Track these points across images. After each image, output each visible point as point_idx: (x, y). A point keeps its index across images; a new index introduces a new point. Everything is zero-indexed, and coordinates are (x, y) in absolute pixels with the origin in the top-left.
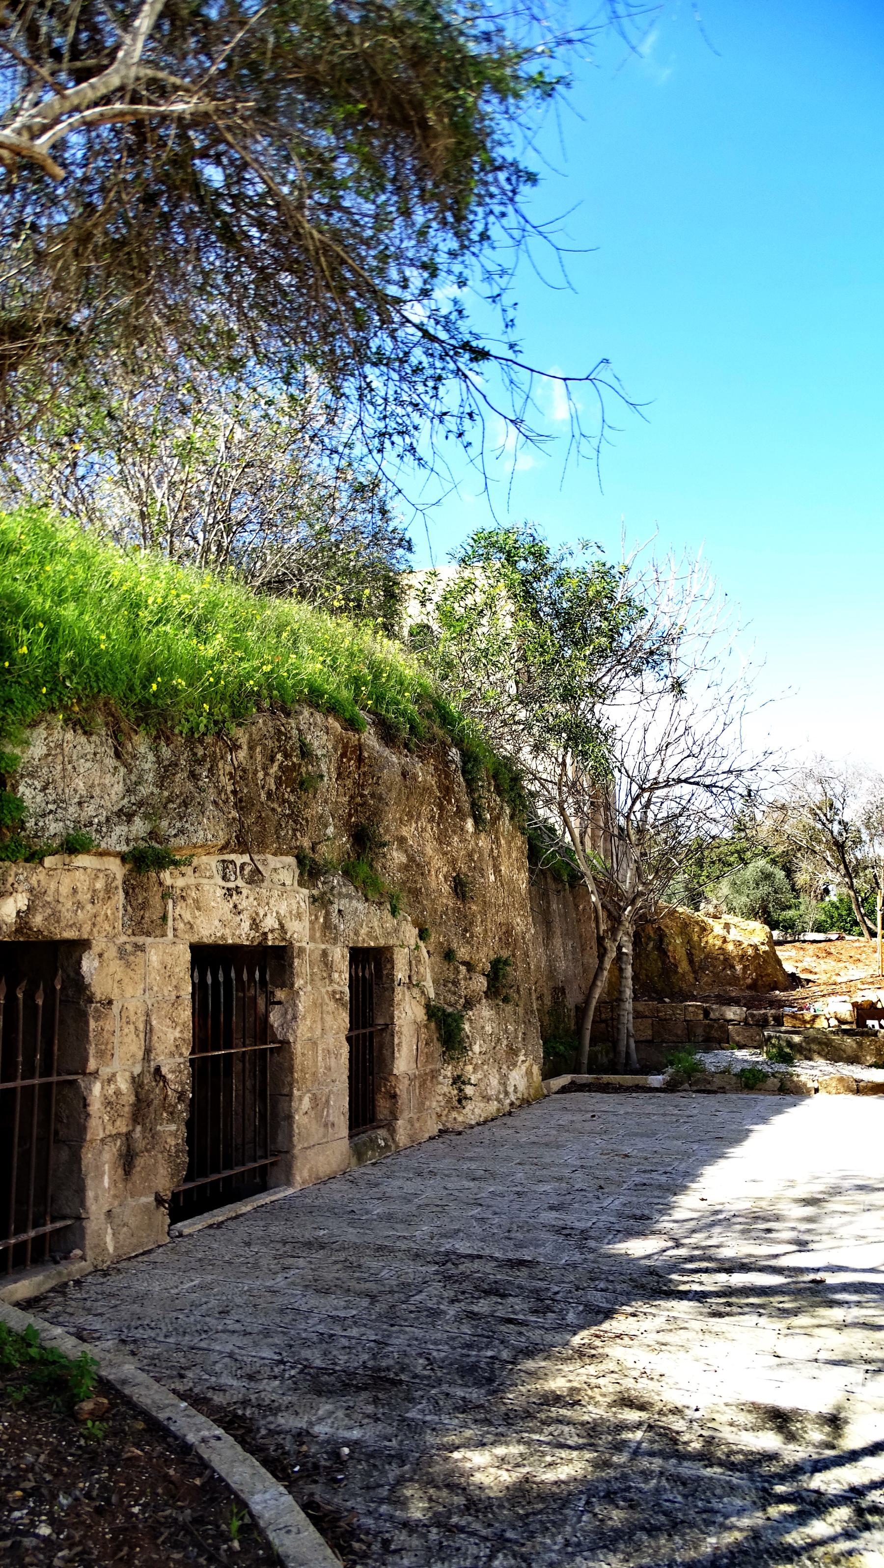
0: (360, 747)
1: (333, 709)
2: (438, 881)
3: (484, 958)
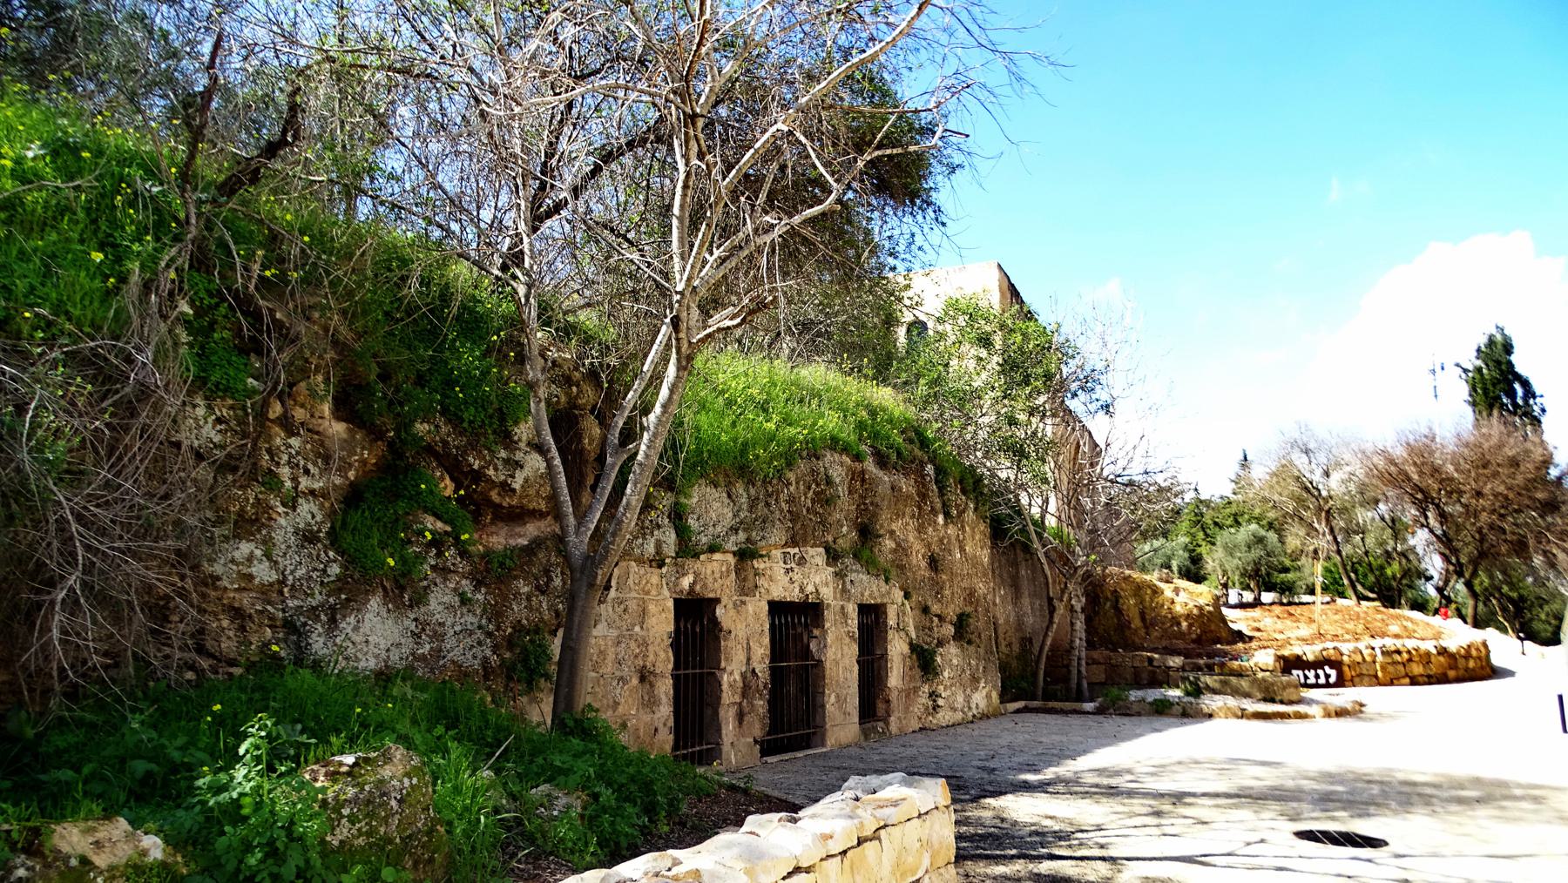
0: (863, 472)
1: (846, 450)
2: (918, 559)
3: (951, 612)
